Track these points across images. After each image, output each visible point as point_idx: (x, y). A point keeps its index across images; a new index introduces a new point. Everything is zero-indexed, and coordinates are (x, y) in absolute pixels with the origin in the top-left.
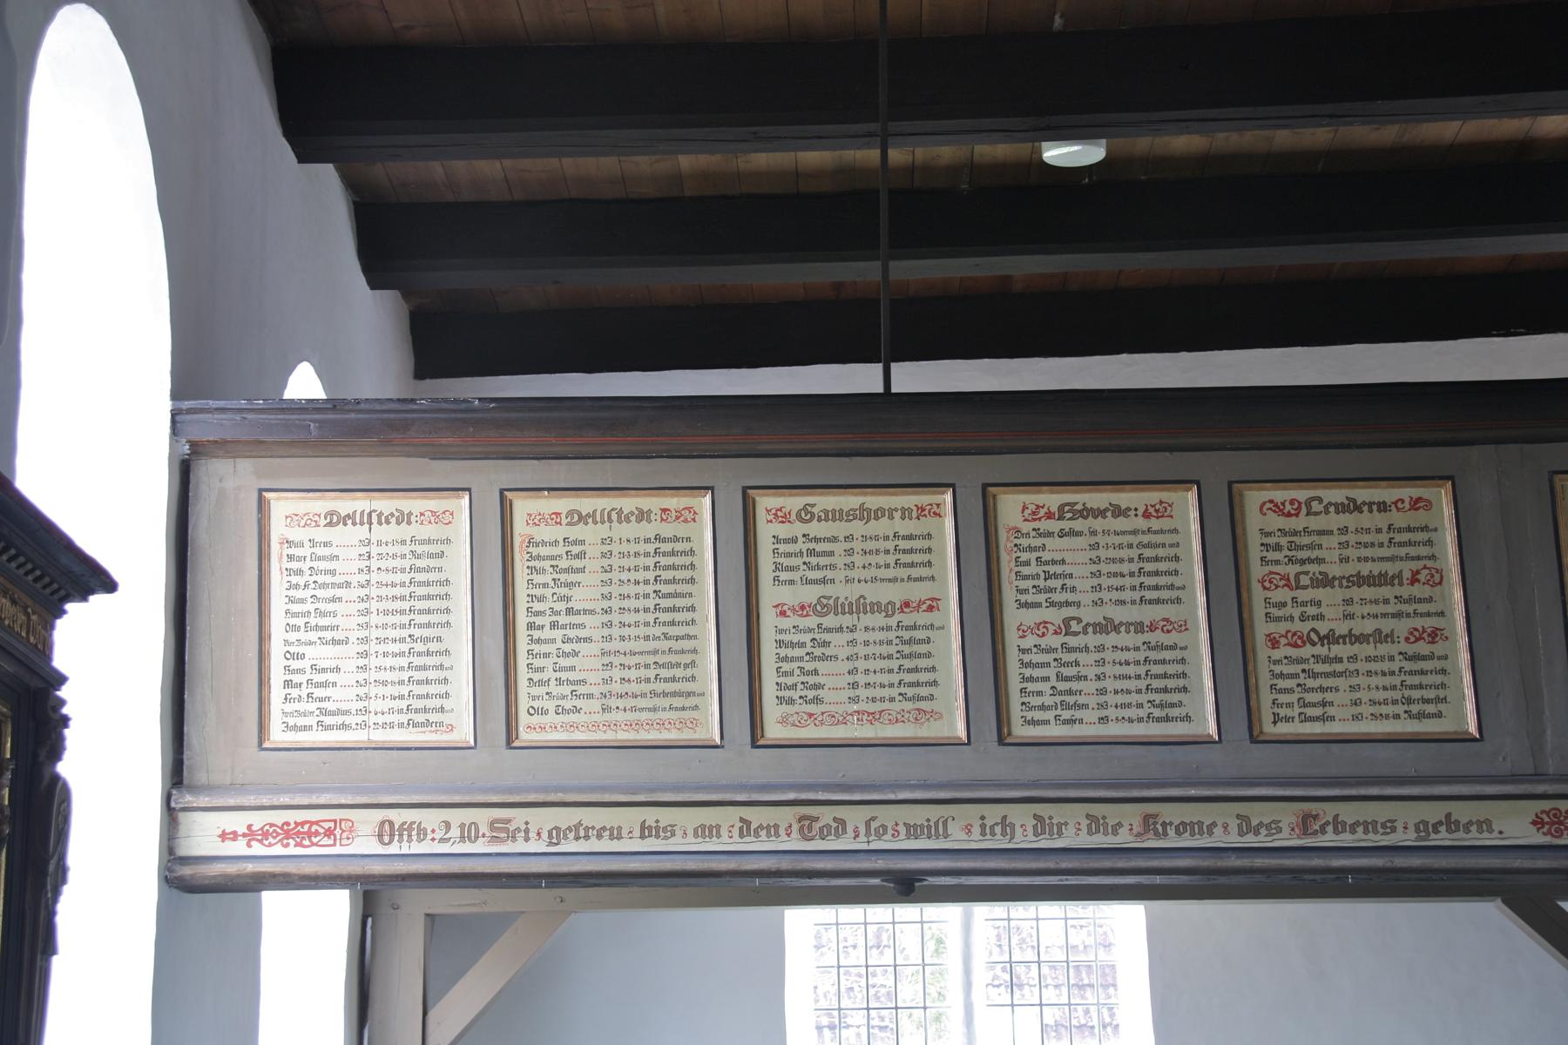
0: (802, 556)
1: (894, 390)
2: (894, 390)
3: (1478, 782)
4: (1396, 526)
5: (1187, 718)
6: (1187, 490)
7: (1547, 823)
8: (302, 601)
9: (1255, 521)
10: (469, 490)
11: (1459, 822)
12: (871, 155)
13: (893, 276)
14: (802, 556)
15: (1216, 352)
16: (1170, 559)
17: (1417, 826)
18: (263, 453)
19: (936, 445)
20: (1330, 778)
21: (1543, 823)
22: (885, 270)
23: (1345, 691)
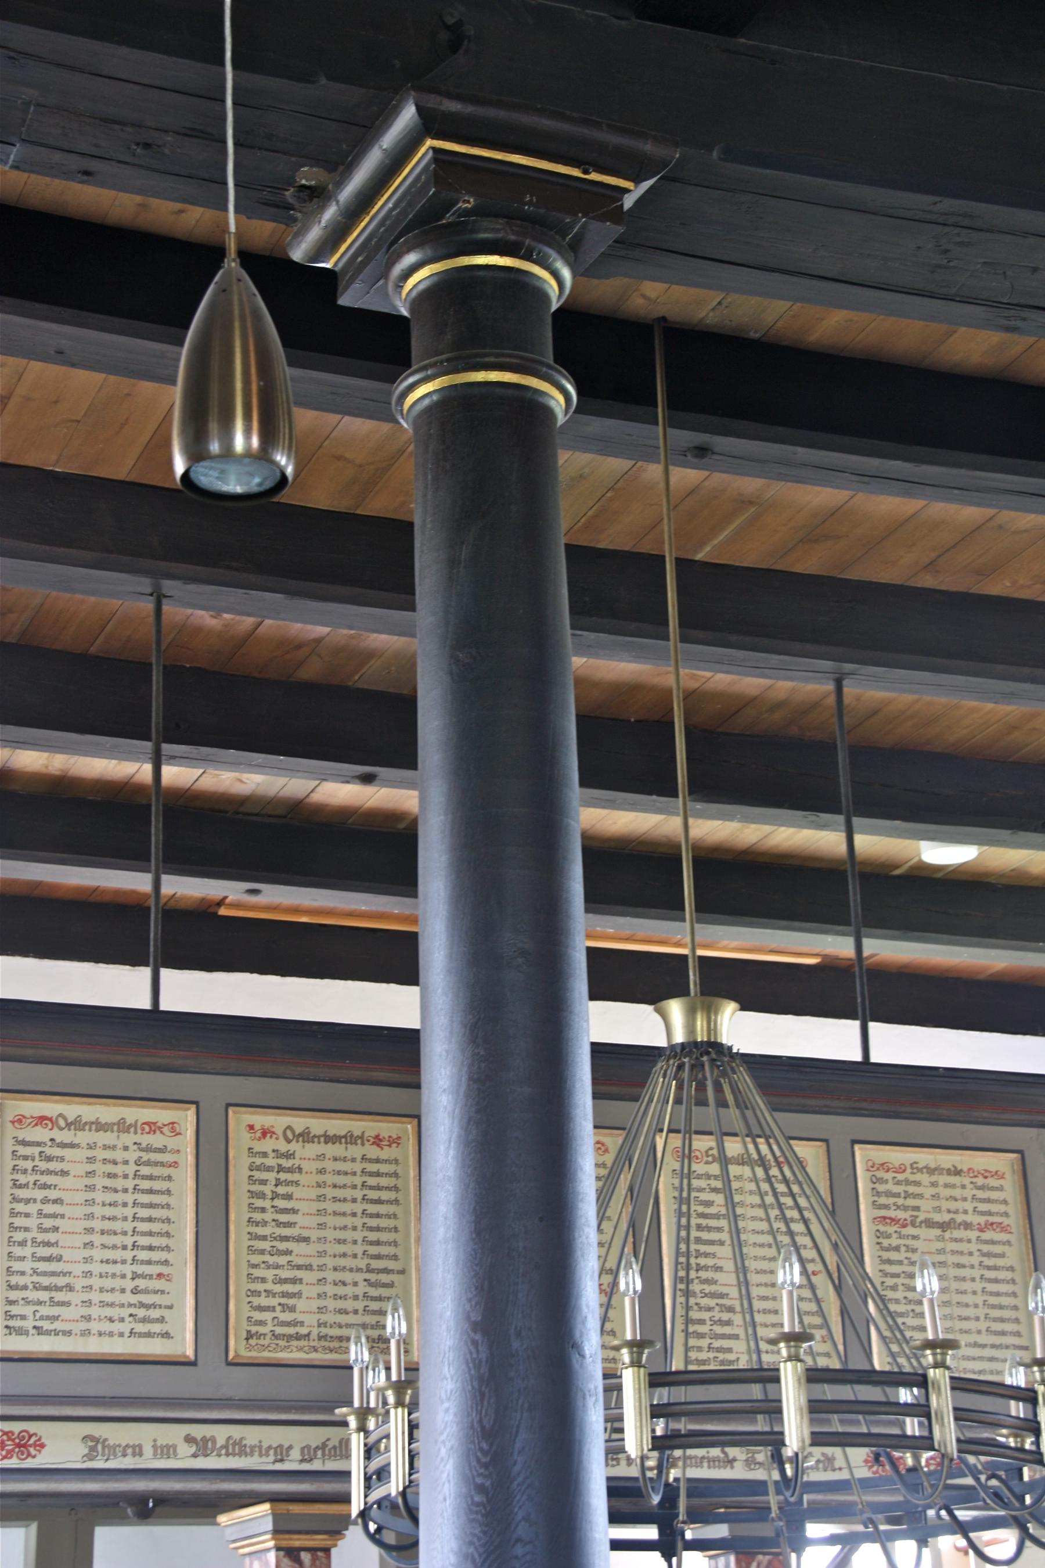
0: (33, 1160)
1: (163, 1007)
2: (163, 1007)
3: (54, 1404)
4: (368, 1157)
5: (166, 1335)
6: (188, 1109)
7: (30, 1446)
8: (263, 1210)
9: (240, 1140)
10: (196, 1103)
11: (310, 1446)
12: (144, 772)
13: (866, 952)
14: (33, 1160)
15: (393, 986)
16: (164, 1179)
17: (302, 1449)
18: (357, 1074)
19: (30, 1052)
20: (317, 1401)
21: (35, 1445)
22: (157, 884)
23: (77, 1305)
